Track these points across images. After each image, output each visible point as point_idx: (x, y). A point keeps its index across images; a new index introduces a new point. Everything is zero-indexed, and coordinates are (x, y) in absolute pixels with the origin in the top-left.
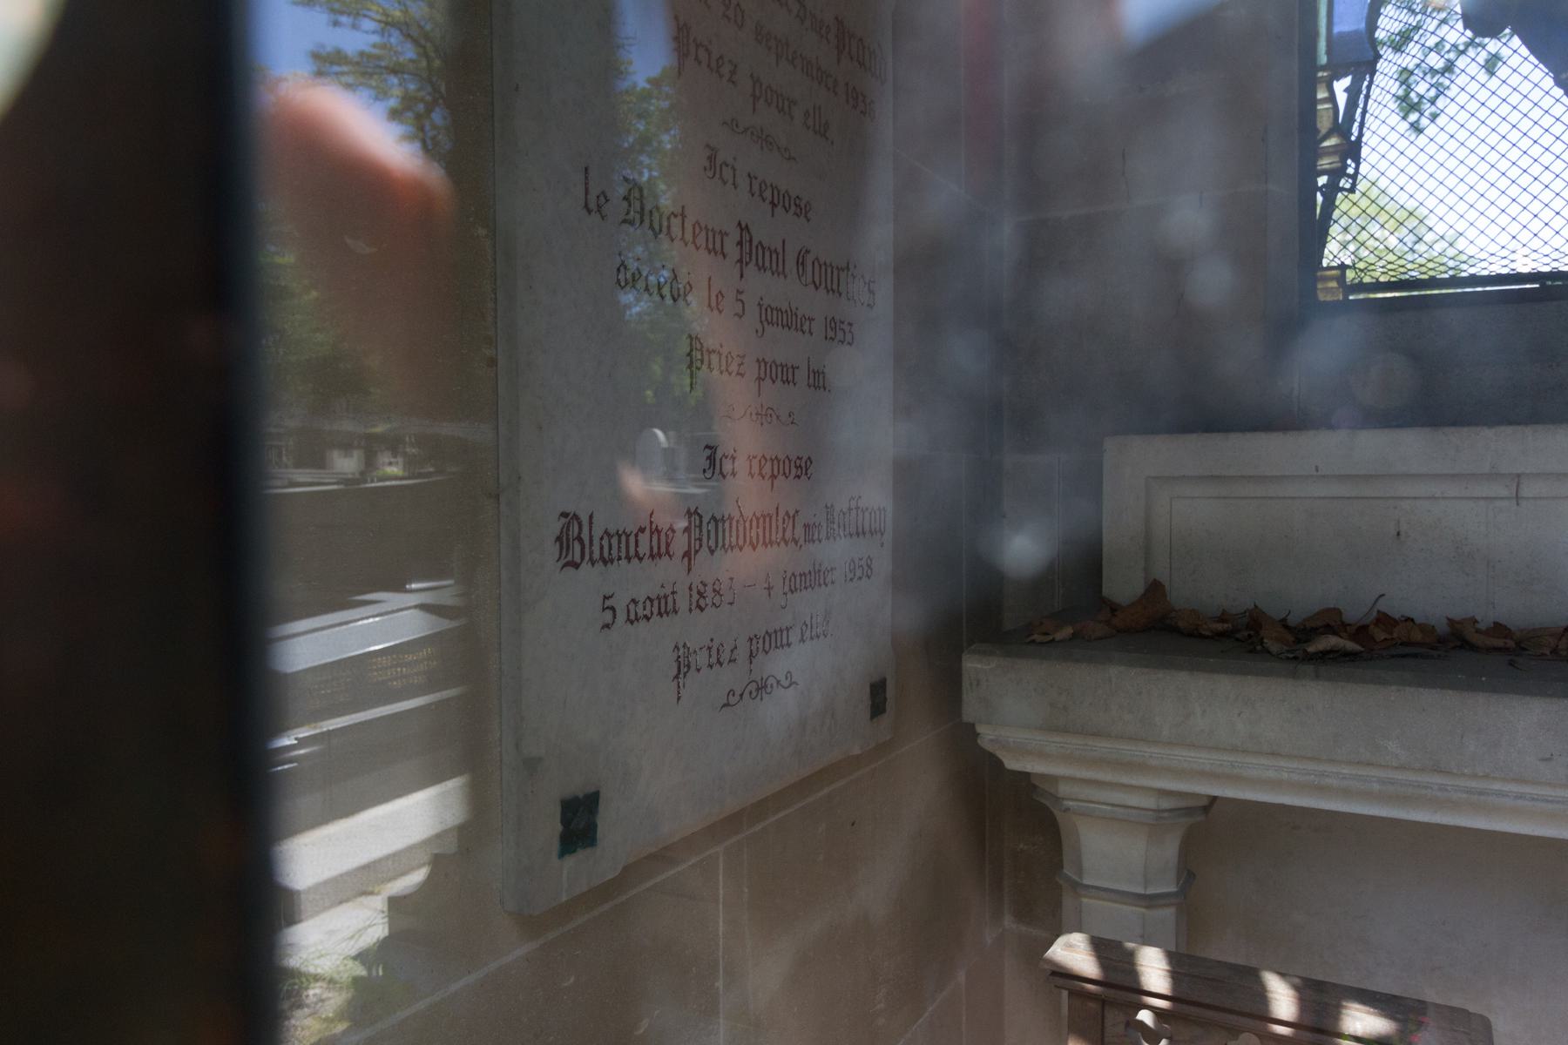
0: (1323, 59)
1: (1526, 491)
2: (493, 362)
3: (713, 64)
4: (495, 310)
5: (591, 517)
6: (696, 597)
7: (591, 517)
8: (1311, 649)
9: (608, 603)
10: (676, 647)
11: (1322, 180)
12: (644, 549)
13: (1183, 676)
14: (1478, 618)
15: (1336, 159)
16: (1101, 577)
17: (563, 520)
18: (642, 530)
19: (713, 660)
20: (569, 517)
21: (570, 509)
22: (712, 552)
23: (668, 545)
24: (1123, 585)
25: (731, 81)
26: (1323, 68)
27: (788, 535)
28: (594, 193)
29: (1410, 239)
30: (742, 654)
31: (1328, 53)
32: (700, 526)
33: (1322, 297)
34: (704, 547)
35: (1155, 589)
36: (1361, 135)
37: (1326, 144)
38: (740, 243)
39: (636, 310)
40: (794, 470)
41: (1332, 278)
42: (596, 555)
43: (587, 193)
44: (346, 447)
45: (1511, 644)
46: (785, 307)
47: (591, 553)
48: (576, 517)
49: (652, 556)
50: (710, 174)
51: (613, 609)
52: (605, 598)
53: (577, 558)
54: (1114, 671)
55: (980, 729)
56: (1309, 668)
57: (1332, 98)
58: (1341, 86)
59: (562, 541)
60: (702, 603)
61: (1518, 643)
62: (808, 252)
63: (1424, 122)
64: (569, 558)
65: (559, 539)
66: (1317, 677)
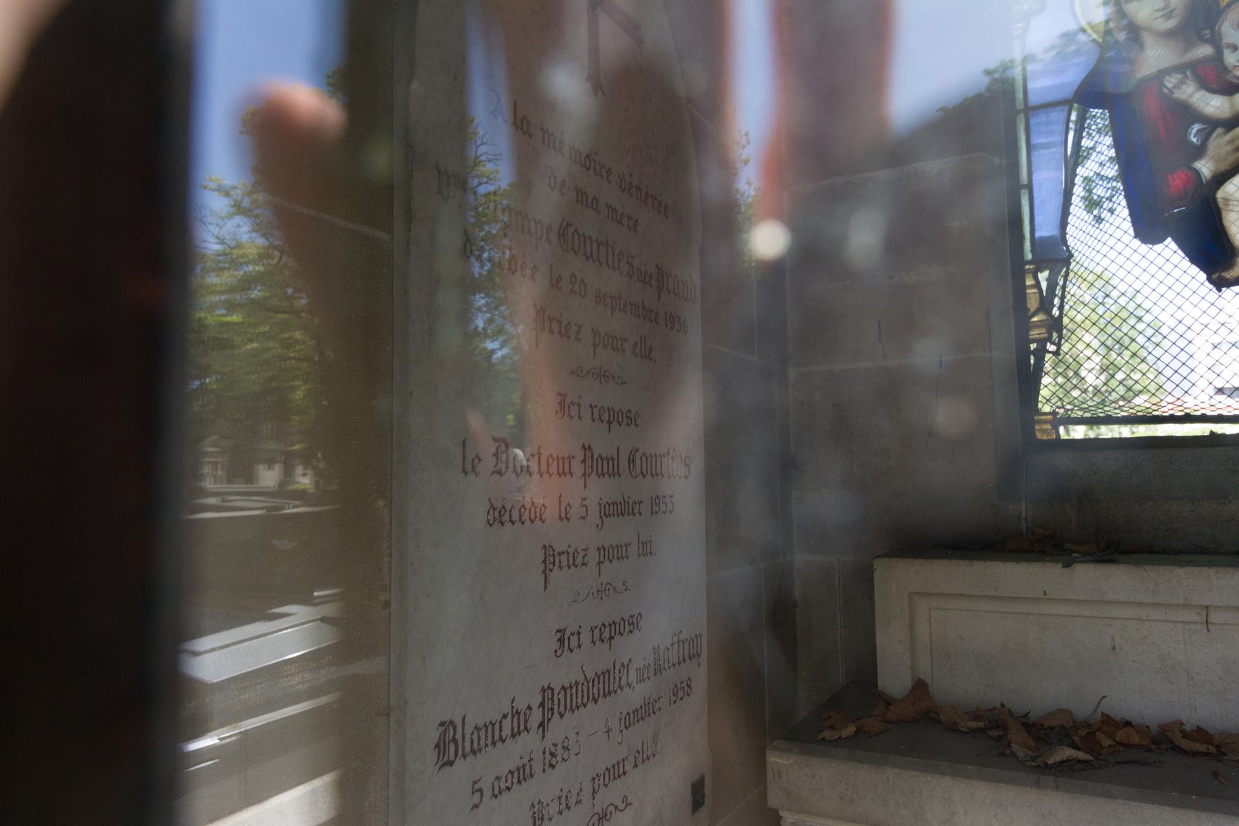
0: (1029, 256)
1: (1214, 618)
2: (387, 604)
3: (563, 331)
4: (390, 562)
5: (464, 719)
6: (548, 756)
7: (464, 719)
8: (1050, 761)
9: (476, 787)
10: (533, 806)
11: (1033, 346)
12: (507, 731)
13: (946, 781)
14: (1184, 720)
15: (1044, 331)
16: (875, 656)
17: (441, 729)
18: (505, 717)
19: (563, 806)
20: (447, 725)
21: (447, 718)
22: (561, 716)
23: (526, 722)
24: (894, 677)
25: (577, 339)
26: (1029, 263)
27: (624, 682)
28: (469, 457)
29: (1100, 296)
30: (586, 796)
31: (1032, 251)
32: (552, 698)
33: (1039, 436)
34: (556, 715)
35: (920, 686)
36: (1061, 308)
37: (1035, 319)
38: (584, 461)
39: (499, 354)
40: (627, 627)
41: (1046, 422)
42: (468, 749)
43: (464, 459)
44: (270, 463)
45: (1212, 749)
46: (620, 499)
47: (463, 748)
48: (452, 723)
49: (513, 736)
50: (560, 415)
51: (481, 790)
52: (475, 782)
53: (452, 757)
54: (890, 772)
55: (782, 813)
56: (1050, 779)
57: (1038, 285)
58: (1043, 276)
59: (440, 747)
60: (554, 762)
61: (1218, 747)
62: (637, 451)
63: (1105, 214)
64: (446, 759)
65: (437, 746)
66: (1057, 788)
